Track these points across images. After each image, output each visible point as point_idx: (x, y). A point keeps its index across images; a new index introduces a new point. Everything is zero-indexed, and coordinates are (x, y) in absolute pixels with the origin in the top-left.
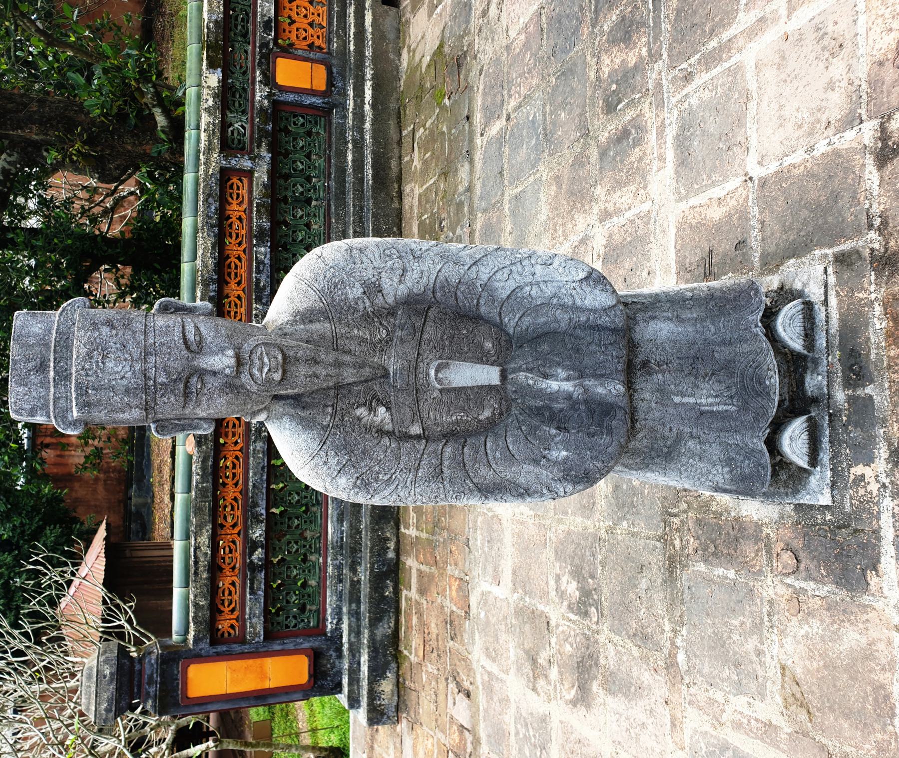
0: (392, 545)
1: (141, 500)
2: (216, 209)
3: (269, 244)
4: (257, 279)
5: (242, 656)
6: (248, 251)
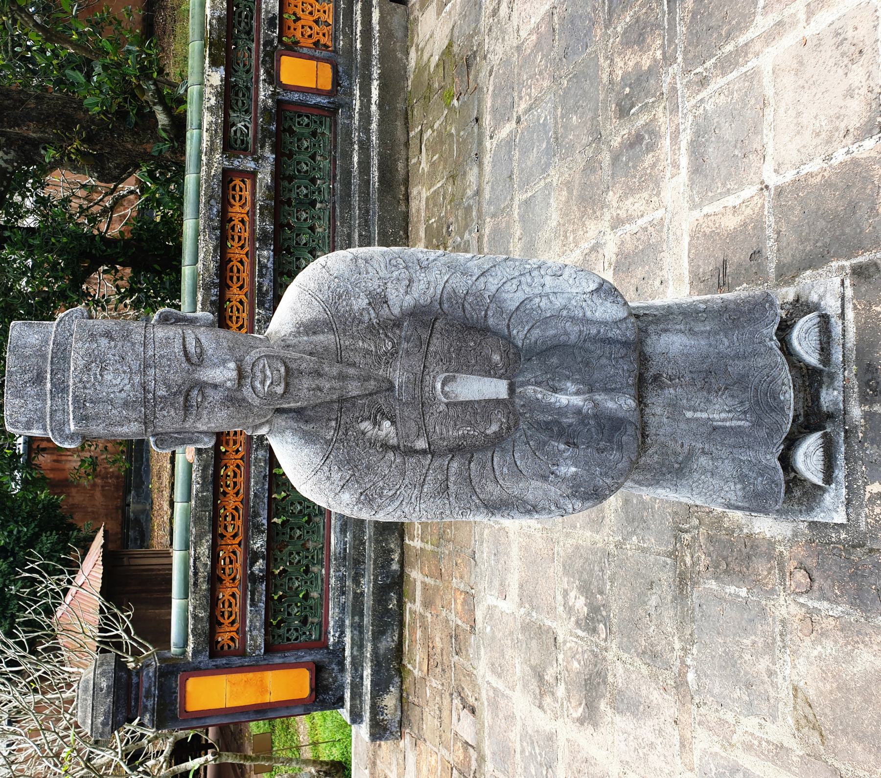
0: (396, 557)
1: (139, 507)
2: (218, 211)
3: (272, 248)
4: (260, 284)
5: (242, 669)
6: (251, 255)
